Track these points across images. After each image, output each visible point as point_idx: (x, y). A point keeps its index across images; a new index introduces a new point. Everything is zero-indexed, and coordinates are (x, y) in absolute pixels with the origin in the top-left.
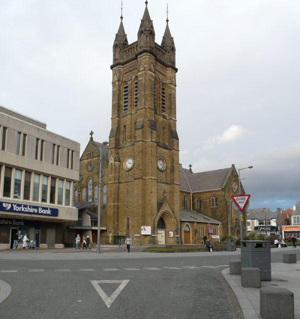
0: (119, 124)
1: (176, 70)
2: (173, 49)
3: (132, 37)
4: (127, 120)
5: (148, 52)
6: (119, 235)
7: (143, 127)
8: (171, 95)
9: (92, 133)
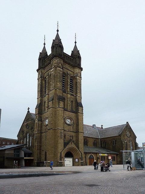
0: (41, 101)
1: (82, 69)
2: (79, 58)
3: (49, 52)
4: (46, 99)
5: (57, 57)
6: (41, 161)
7: (53, 100)
8: (77, 82)
9: (29, 109)
